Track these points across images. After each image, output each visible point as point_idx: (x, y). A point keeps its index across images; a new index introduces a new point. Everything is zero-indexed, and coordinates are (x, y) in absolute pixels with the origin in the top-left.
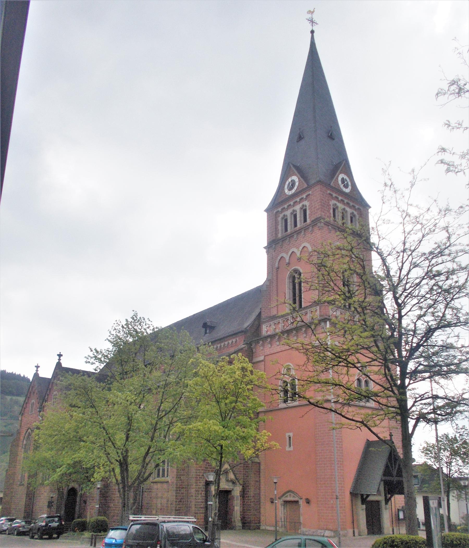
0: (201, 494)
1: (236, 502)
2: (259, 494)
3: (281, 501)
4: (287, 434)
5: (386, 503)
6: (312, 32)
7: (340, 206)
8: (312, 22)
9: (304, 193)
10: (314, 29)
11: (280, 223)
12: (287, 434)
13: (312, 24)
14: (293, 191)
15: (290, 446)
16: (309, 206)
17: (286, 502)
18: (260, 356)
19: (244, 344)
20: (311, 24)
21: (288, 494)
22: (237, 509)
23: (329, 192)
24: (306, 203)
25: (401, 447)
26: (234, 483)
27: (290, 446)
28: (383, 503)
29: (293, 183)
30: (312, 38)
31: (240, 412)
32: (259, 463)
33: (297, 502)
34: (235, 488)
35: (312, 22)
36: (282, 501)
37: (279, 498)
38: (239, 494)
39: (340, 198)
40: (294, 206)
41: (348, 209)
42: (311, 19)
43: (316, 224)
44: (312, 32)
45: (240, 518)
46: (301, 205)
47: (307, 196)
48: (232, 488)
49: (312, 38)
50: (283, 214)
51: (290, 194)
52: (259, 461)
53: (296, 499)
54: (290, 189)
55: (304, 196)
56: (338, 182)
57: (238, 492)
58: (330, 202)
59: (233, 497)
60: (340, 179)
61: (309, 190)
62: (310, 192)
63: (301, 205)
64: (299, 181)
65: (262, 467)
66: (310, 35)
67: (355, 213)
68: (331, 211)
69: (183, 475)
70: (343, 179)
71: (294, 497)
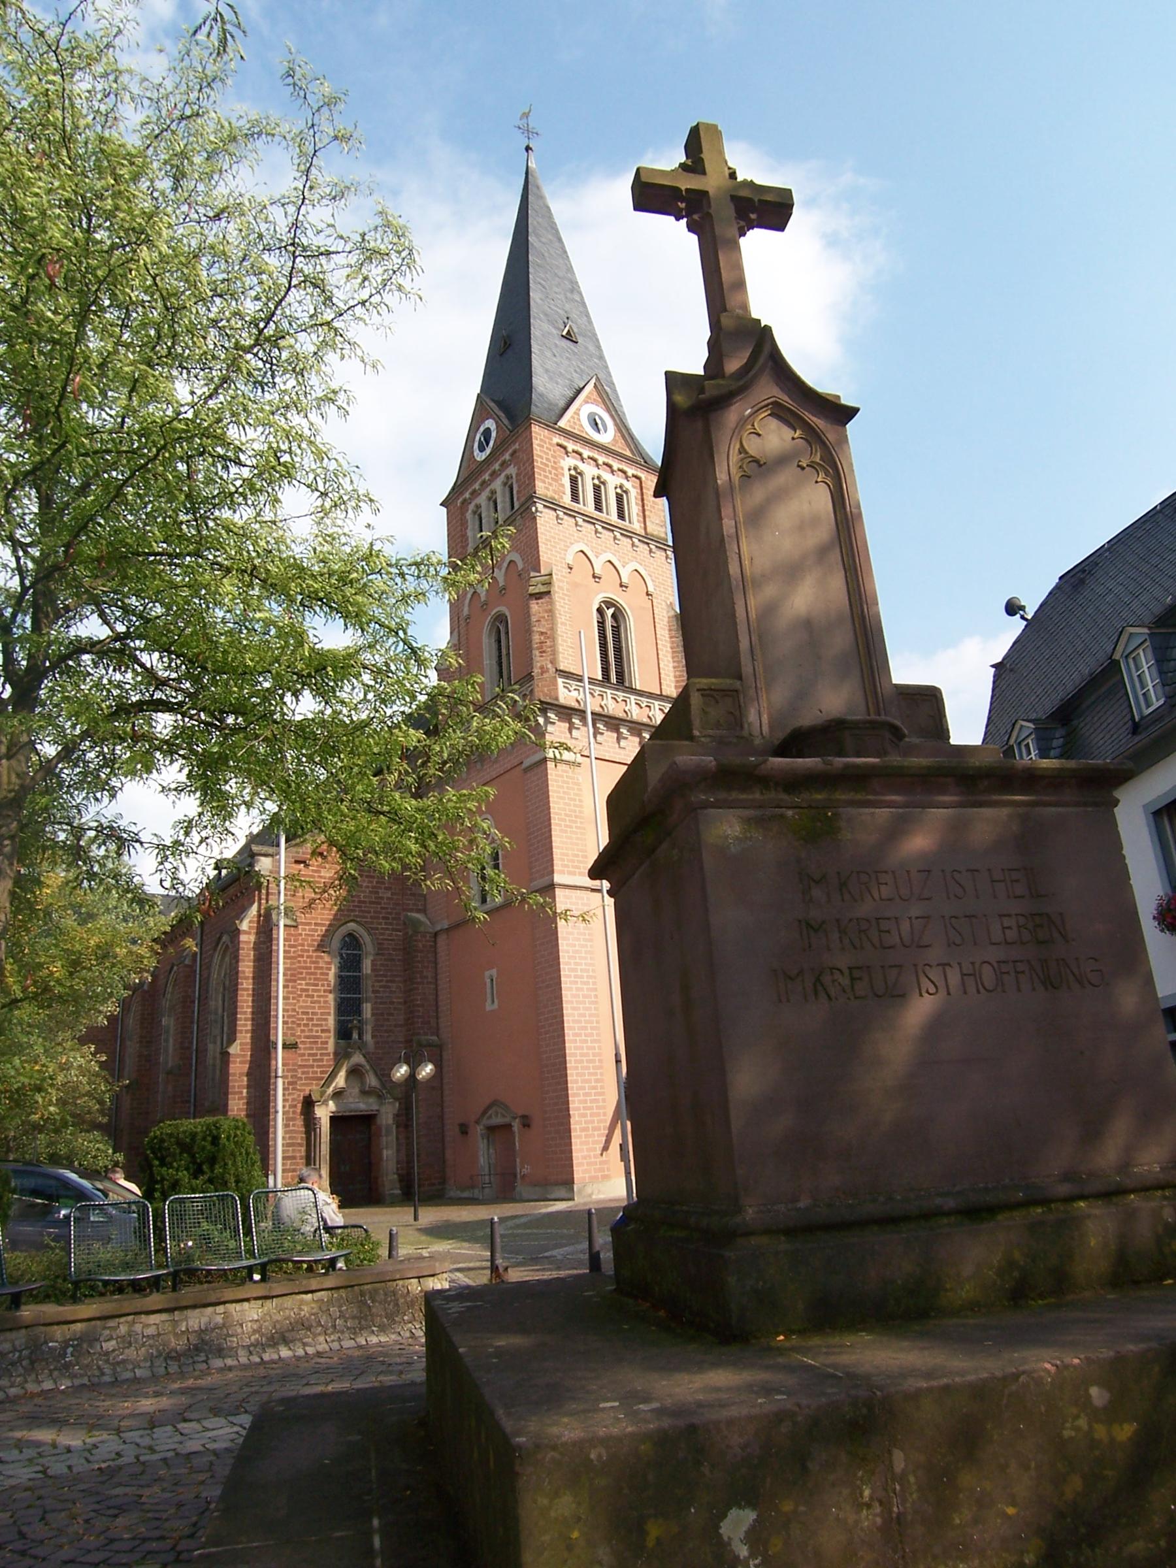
1: (384, 1138)
3: (479, 1129)
4: (487, 973)
7: (589, 471)
8: (528, 132)
9: (506, 450)
11: (469, 523)
14: (488, 451)
15: (493, 1002)
16: (517, 475)
17: (491, 1129)
22: (389, 1155)
26: (380, 1097)
27: (493, 1002)
29: (487, 432)
31: (149, 471)
33: (508, 1127)
34: (383, 1110)
35: (528, 132)
36: (482, 1127)
37: (477, 1122)
38: (390, 1121)
40: (491, 481)
41: (606, 476)
45: (396, 1176)
46: (502, 477)
47: (512, 455)
48: (375, 1107)
50: (473, 504)
51: (484, 458)
53: (507, 1120)
54: (482, 449)
55: (507, 456)
57: (390, 1116)
58: (562, 461)
59: (379, 1128)
61: (514, 442)
62: (517, 446)
63: (502, 477)
64: (497, 427)
67: (628, 485)
68: (566, 482)
71: (504, 1116)
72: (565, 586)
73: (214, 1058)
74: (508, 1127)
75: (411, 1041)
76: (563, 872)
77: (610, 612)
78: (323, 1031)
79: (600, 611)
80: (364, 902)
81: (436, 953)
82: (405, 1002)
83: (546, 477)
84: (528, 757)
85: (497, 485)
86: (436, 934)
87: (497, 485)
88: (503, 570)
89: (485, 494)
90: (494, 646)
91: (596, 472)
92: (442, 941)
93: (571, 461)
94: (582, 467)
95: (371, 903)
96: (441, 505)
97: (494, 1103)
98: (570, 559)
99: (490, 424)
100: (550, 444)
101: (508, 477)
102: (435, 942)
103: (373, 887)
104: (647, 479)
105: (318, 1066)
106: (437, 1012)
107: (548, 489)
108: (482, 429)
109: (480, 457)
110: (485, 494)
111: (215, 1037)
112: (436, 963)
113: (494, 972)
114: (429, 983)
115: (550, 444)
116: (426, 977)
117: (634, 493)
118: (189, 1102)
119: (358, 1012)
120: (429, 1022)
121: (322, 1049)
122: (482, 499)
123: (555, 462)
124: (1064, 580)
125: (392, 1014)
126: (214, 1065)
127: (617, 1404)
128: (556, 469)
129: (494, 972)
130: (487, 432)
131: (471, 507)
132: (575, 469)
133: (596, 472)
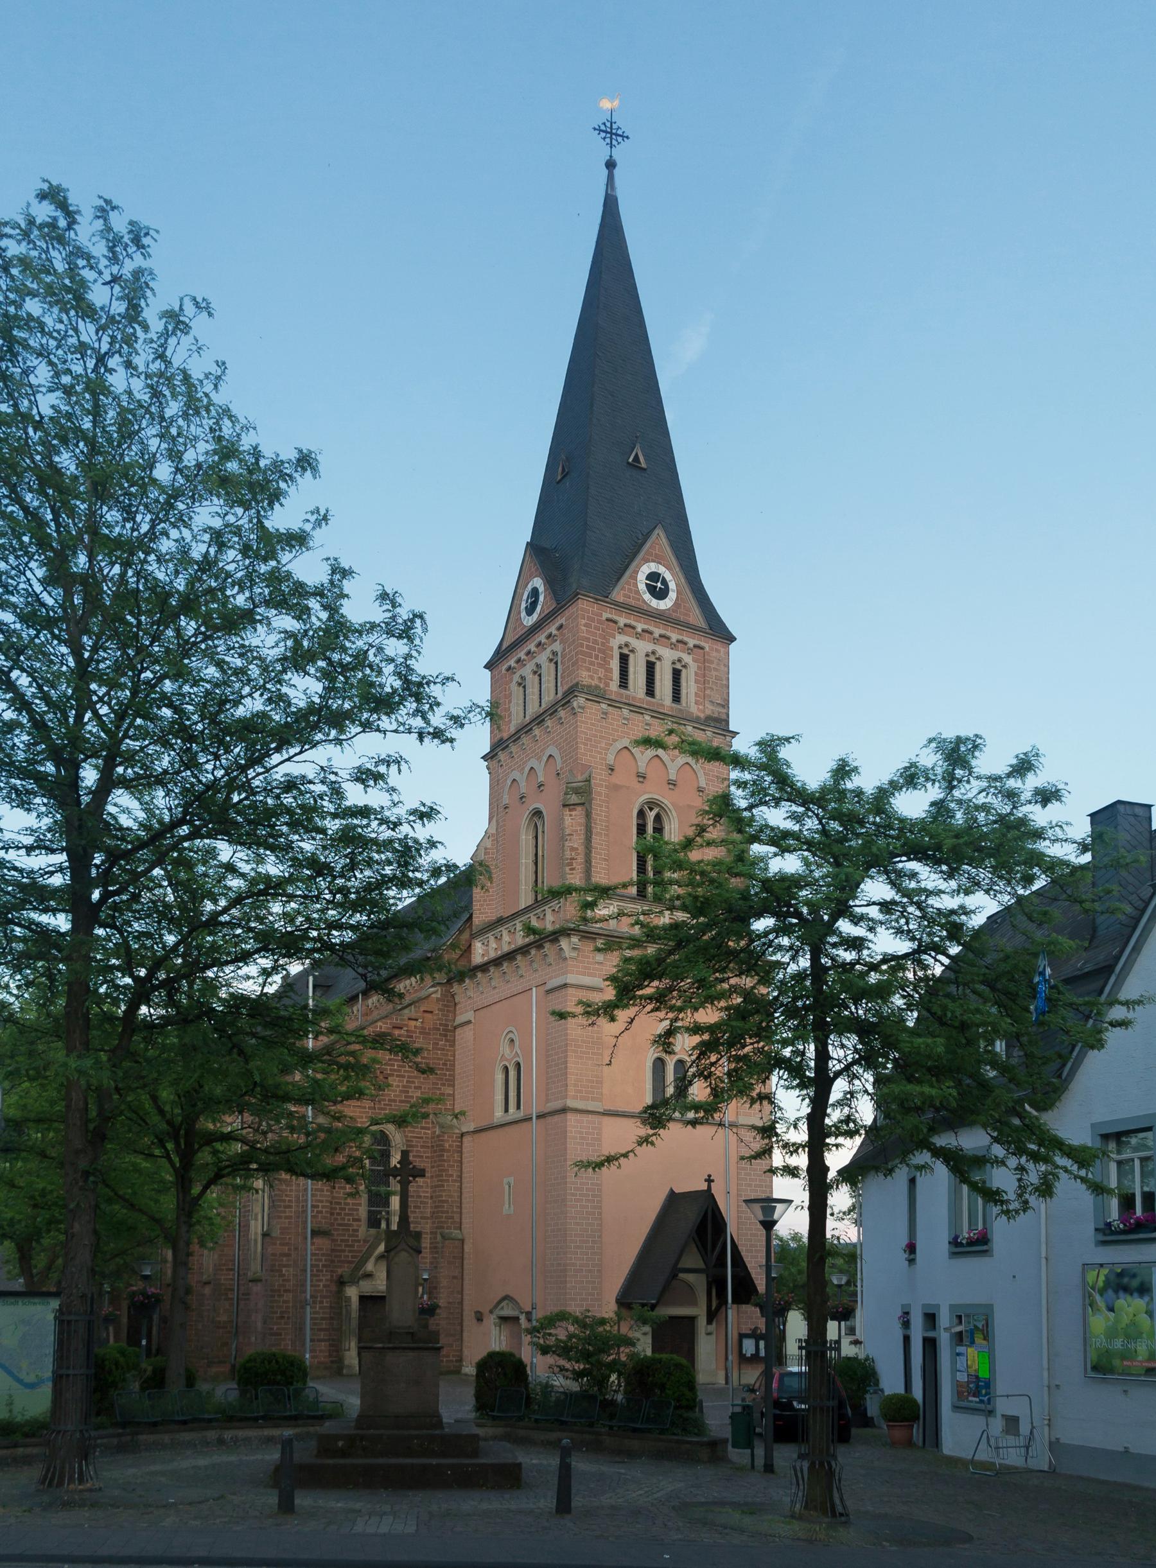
0: (321, 1302)
2: (461, 1303)
5: (709, 1322)
6: (611, 165)
10: (615, 157)
12: (505, 1180)
13: (611, 139)
17: (504, 1319)
18: (467, 1011)
19: (432, 986)
20: (608, 140)
21: (504, 1304)
23: (605, 615)
24: (557, 646)
25: (807, 1204)
28: (702, 1322)
29: (535, 592)
30: (611, 179)
32: (463, 1241)
37: (491, 1312)
39: (640, 627)
42: (608, 124)
43: (569, 701)
44: (611, 165)
49: (611, 179)
52: (460, 1237)
56: (636, 585)
60: (642, 577)
65: (467, 1248)
66: (606, 172)
67: (687, 659)
68: (615, 665)
69: (285, 1266)
70: (653, 576)
72: (603, 790)
73: (256, 1233)
74: (517, 1319)
75: (436, 1233)
76: (575, 1098)
77: (651, 815)
78: (354, 1220)
79: (641, 814)
80: (395, 1101)
81: (461, 1152)
82: (432, 1197)
83: (592, 663)
84: (551, 978)
85: (543, 658)
86: (462, 1135)
87: (543, 658)
88: (543, 763)
89: (530, 666)
90: (532, 842)
91: (650, 647)
92: (466, 1139)
93: (621, 639)
94: (634, 643)
95: (401, 1101)
96: (485, 667)
97: (506, 1298)
98: (611, 759)
99: (538, 583)
100: (599, 622)
101: (554, 653)
102: (461, 1142)
103: (404, 1086)
104: (711, 649)
105: (350, 1251)
106: (461, 1207)
107: (591, 677)
108: (530, 587)
109: (529, 621)
110: (530, 666)
111: (256, 1215)
112: (461, 1162)
113: (511, 1180)
114: (453, 1181)
115: (599, 622)
116: (452, 1176)
117: (693, 667)
118: (233, 1270)
119: (387, 1204)
120: (452, 1218)
121: (353, 1236)
122: (527, 671)
123: (603, 644)
124: (1121, 808)
125: (419, 1207)
126: (256, 1241)
127: (111, 1329)
128: (603, 652)
129: (511, 1180)
130: (535, 592)
131: (516, 678)
132: (627, 645)
133: (650, 647)
